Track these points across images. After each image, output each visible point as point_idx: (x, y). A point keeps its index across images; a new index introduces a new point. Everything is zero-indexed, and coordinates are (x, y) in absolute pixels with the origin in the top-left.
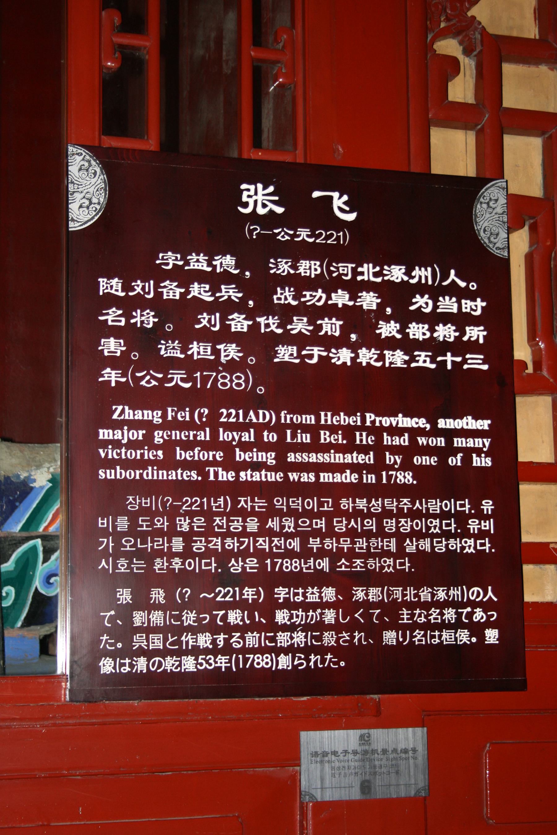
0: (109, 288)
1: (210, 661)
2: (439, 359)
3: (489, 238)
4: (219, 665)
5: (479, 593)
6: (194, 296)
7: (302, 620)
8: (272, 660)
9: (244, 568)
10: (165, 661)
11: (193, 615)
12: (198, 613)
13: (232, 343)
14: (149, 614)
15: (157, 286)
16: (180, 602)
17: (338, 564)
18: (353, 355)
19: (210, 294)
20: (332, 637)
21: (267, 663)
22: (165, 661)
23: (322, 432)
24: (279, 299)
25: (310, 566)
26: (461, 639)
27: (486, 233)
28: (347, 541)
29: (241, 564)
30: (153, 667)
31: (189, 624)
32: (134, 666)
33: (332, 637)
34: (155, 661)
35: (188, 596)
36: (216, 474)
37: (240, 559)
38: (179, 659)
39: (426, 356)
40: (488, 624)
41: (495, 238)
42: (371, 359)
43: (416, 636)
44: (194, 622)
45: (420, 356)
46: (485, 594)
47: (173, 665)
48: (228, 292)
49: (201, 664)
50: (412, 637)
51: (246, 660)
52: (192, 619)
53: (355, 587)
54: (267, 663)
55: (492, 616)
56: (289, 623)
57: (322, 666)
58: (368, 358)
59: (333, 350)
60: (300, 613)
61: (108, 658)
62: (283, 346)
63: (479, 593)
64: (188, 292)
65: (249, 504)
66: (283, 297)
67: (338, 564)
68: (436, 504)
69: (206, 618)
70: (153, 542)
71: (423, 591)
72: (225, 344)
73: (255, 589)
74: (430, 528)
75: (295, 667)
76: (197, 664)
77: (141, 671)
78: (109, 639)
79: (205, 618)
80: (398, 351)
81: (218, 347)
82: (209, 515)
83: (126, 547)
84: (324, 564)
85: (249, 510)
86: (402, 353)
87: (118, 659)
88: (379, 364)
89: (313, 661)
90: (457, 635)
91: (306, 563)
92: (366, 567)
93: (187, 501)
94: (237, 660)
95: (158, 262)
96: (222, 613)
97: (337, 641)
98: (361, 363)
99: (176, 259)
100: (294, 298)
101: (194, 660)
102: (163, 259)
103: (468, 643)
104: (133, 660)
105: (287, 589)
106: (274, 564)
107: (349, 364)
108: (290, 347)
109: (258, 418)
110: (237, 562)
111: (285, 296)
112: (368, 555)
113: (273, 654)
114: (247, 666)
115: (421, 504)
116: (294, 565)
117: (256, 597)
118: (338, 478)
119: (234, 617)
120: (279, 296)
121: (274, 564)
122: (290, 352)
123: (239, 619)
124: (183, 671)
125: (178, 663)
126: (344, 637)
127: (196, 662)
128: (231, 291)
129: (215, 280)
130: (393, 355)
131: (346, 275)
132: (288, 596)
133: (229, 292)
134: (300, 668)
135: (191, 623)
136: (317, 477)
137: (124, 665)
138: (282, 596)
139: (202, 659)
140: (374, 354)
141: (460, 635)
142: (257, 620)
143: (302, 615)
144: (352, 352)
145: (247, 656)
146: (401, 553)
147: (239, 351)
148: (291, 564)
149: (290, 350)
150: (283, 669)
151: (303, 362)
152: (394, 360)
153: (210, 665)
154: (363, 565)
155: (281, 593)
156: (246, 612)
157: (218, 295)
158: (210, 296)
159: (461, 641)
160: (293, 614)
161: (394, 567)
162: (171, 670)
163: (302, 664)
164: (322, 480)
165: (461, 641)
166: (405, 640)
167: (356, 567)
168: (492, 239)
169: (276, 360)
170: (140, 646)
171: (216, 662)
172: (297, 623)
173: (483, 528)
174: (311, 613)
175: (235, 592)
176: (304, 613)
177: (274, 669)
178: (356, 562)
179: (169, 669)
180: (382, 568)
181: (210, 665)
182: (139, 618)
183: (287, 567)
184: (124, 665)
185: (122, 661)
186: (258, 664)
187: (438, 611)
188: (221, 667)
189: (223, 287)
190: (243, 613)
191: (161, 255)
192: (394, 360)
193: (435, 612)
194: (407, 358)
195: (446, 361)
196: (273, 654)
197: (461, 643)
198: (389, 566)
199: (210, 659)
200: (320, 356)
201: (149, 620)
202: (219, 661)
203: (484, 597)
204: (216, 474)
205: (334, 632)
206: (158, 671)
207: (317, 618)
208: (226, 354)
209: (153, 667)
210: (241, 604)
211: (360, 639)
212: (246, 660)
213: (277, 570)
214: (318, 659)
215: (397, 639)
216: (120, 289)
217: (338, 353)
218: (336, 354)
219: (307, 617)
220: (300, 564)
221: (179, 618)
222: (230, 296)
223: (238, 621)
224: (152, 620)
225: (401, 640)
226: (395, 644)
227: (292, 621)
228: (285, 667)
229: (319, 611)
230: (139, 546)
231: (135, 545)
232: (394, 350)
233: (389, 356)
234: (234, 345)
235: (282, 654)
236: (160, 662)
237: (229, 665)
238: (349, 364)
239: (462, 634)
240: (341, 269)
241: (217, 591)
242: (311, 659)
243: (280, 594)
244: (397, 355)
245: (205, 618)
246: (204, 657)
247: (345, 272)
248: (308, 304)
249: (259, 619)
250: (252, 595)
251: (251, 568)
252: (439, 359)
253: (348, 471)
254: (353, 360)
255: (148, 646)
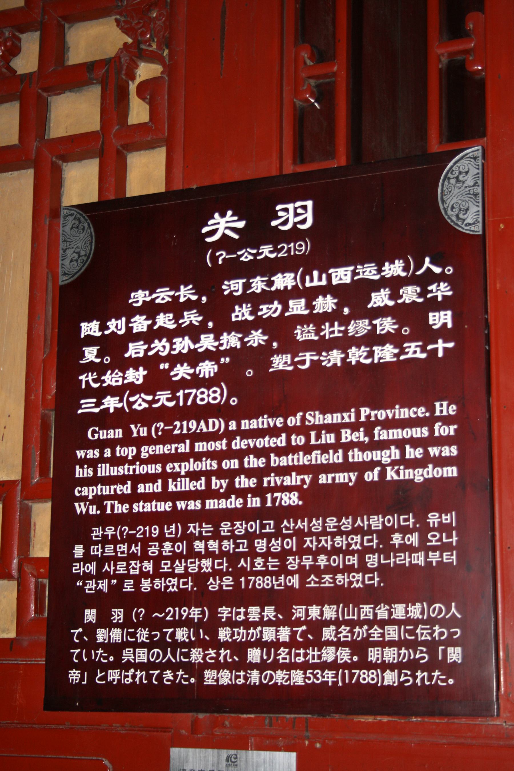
0: (89, 330)
1: (318, 676)
2: (430, 347)
3: (457, 216)
4: (326, 679)
5: (440, 610)
6: (160, 327)
7: (243, 638)
8: (377, 676)
9: (221, 586)
10: (276, 674)
11: (146, 632)
12: (150, 631)
13: (387, 316)
14: (109, 632)
15: (128, 322)
16: (135, 621)
17: (308, 580)
18: (343, 356)
19: (173, 321)
20: (200, 654)
21: (373, 679)
22: (276, 674)
23: (343, 431)
24: (237, 316)
25: (281, 583)
26: (342, 657)
27: (454, 210)
28: (309, 559)
29: (218, 582)
30: (265, 680)
31: (142, 641)
32: (248, 678)
33: (200, 654)
34: (267, 674)
35: (143, 616)
36: (113, 507)
37: (217, 577)
38: (288, 673)
39: (417, 346)
40: (451, 642)
41: (464, 214)
42: (360, 357)
43: (280, 654)
44: (147, 638)
45: (410, 347)
46: (448, 610)
47: (283, 678)
48: (190, 317)
49: (309, 678)
50: (276, 655)
51: (352, 675)
52: (145, 636)
53: (296, 606)
54: (373, 679)
55: (456, 633)
56: (230, 640)
57: (429, 683)
58: (357, 356)
59: (324, 354)
60: (241, 631)
61: (225, 670)
62: (278, 356)
63: (440, 610)
64: (154, 323)
65: (198, 529)
66: (240, 314)
67: (308, 580)
68: (378, 520)
69: (157, 635)
70: (395, 557)
71: (380, 609)
72: (380, 319)
73: (200, 609)
74: (203, 568)
75: (401, 684)
76: (305, 678)
77: (255, 683)
78: (104, 653)
79: (156, 635)
80: (388, 345)
81: (374, 322)
82: (190, 539)
83: (431, 541)
84: (294, 581)
85: (197, 535)
86: (392, 346)
87: (234, 671)
88: (368, 361)
89: (419, 678)
90: (338, 653)
91: (277, 580)
92: (334, 582)
93: (140, 529)
94: (344, 675)
95: (130, 301)
96: (171, 630)
97: (204, 658)
98: (351, 362)
99: (145, 296)
100: (251, 313)
101: (303, 674)
102: (134, 298)
103: (349, 661)
104: (247, 673)
105: (229, 609)
106: (248, 582)
107: (339, 365)
108: (284, 356)
109: (208, 427)
110: (215, 580)
111: (242, 313)
112: (334, 571)
113: (379, 670)
114: (353, 682)
115: (363, 521)
116: (266, 582)
117: (201, 616)
118: (223, 504)
119: (181, 634)
120: (237, 313)
121: (248, 582)
122: (284, 361)
123: (185, 637)
124: (292, 684)
125: (287, 677)
126: (210, 654)
127: (304, 676)
128: (192, 316)
129: (176, 308)
130: (382, 350)
131: (237, 291)
132: (230, 615)
133: (191, 318)
134: (406, 685)
135: (144, 640)
136: (203, 504)
137: (239, 677)
138: (225, 615)
139: (310, 673)
140: (364, 351)
141: (341, 653)
142: (202, 637)
143: (243, 633)
144: (342, 353)
145: (353, 671)
146: (363, 568)
147: (394, 324)
148: (264, 582)
149: (442, 317)
150: (389, 685)
151: (296, 368)
152: (383, 355)
153: (318, 679)
154: (331, 581)
155: (224, 612)
156: (192, 630)
157: (181, 321)
158: (174, 323)
159: (342, 659)
160: (234, 631)
161: (363, 582)
162: (281, 683)
163: (408, 681)
164: (207, 507)
165: (342, 659)
166: (269, 658)
167: (325, 583)
168: (461, 216)
169: (271, 370)
170: (128, 659)
171: (323, 677)
172: (238, 641)
173: (444, 521)
174: (251, 631)
175: (175, 611)
176: (245, 631)
177: (379, 685)
178: (325, 578)
179: (279, 681)
180: (167, 587)
181: (318, 679)
182: (101, 635)
183: (260, 585)
184: (239, 677)
185: (237, 673)
186: (364, 679)
187: (348, 628)
188: (328, 682)
189: (185, 313)
190: (189, 631)
191: (133, 294)
192: (383, 355)
193: (345, 630)
194: (396, 351)
195: (437, 349)
196: (379, 670)
197: (342, 662)
198: (173, 586)
199: (318, 673)
200: (312, 360)
201: (109, 637)
202: (326, 676)
203: (447, 614)
204: (113, 507)
205: (201, 649)
206: (270, 684)
207: (257, 635)
208: (381, 328)
209: (265, 679)
210: (188, 623)
211: (225, 656)
212: (352, 675)
213: (250, 587)
214: (424, 676)
215: (262, 657)
216: (97, 330)
217: (329, 355)
218: (326, 357)
219: (248, 634)
220: (272, 581)
221: (133, 635)
222: (191, 321)
223: (185, 638)
224: (112, 637)
225: (265, 657)
226: (259, 661)
227: (234, 638)
228: (391, 684)
229: (259, 628)
230: (445, 540)
231: (440, 539)
232: (383, 345)
233: (378, 352)
234: (389, 319)
235: (388, 671)
236: (271, 675)
237: (335, 680)
238: (339, 365)
239: (344, 652)
240: (232, 286)
241: (167, 611)
242: (417, 676)
243: (223, 613)
244: (387, 349)
245: (156, 635)
246: (311, 671)
247: (236, 289)
248: (264, 317)
249: (204, 636)
250: (198, 614)
251: (227, 586)
252: (430, 347)
253: (430, 466)
254: (343, 360)
255: (135, 660)
